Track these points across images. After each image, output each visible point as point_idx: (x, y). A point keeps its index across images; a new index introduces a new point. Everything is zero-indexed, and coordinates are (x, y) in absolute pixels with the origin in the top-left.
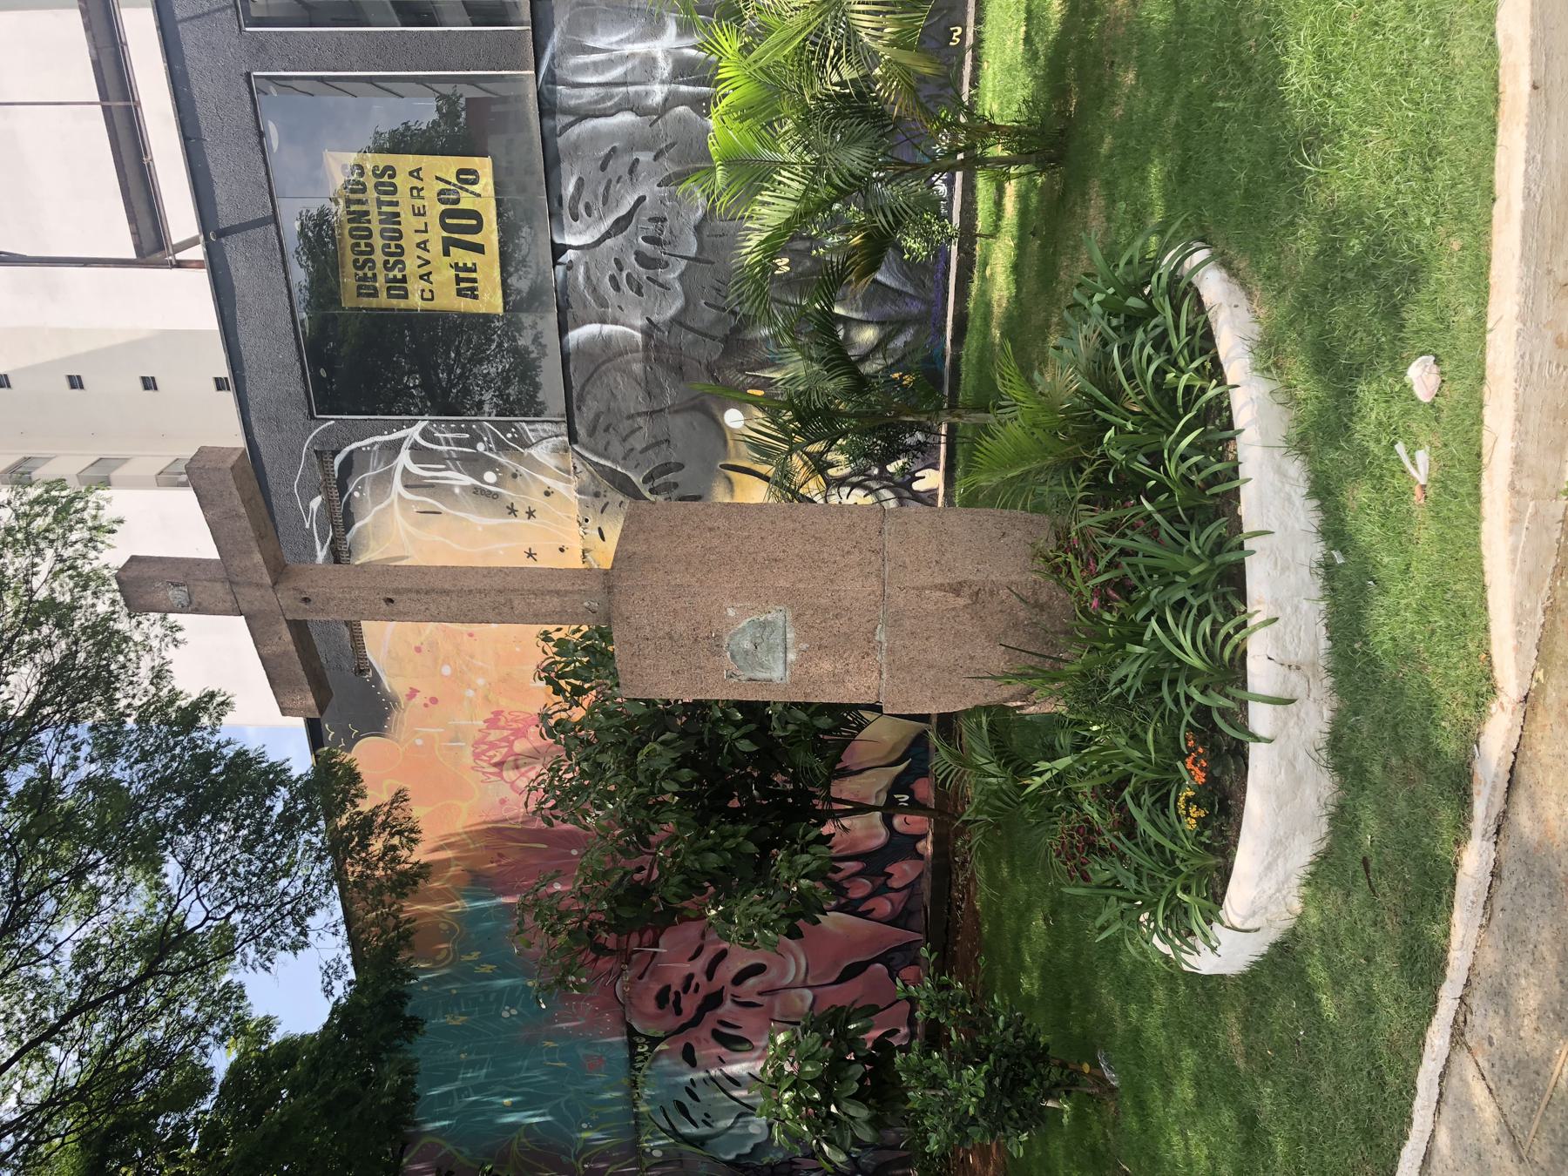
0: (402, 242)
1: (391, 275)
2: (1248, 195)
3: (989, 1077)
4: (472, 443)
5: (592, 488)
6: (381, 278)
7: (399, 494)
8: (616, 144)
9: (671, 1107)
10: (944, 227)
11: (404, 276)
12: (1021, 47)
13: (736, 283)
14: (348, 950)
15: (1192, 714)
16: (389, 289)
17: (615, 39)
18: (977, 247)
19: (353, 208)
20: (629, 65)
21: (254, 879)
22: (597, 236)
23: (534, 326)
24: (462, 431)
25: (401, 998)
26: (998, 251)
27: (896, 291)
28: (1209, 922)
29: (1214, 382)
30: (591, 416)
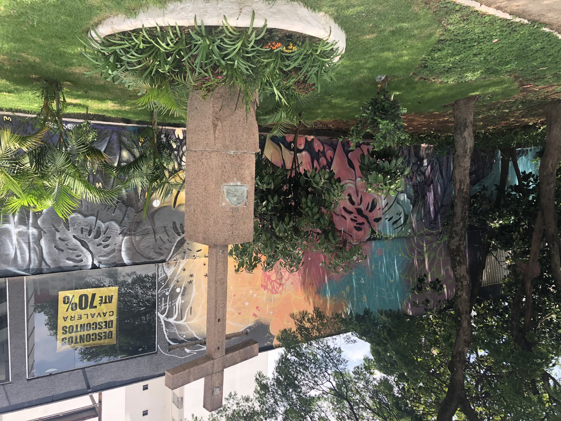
0: (92, 323)
1: (104, 327)
2: (70, 15)
3: (382, 119)
5: (182, 254)
6: (105, 330)
7: (185, 322)
8: (53, 246)
9: (395, 226)
10: (84, 126)
11: (104, 322)
12: (12, 94)
13: (106, 201)
14: (341, 335)
15: (258, 46)
16: (109, 327)
18: (92, 113)
19: (78, 340)
20: (21, 241)
21: (317, 366)
22: (89, 253)
23: (124, 277)
24: (161, 300)
25: (358, 316)
26: (93, 106)
27: (108, 143)
28: (328, 43)
29: (140, 32)
30: (156, 255)
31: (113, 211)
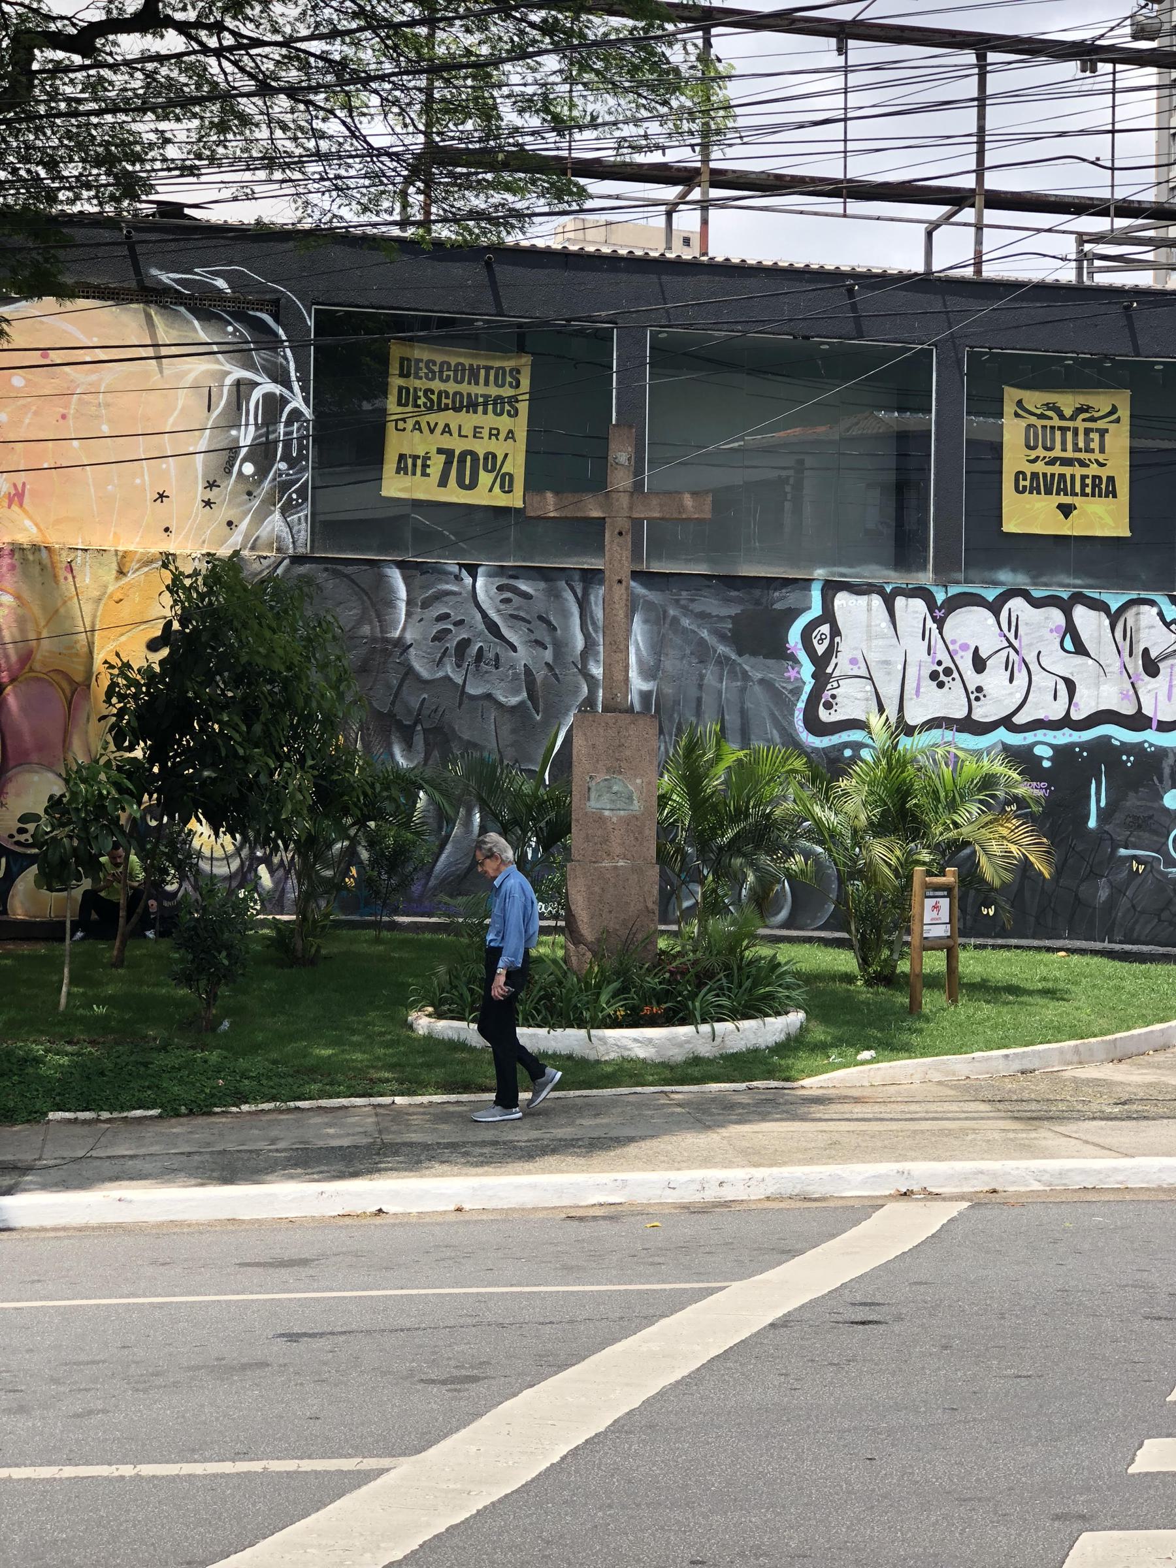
4: (286, 457)
7: (229, 373)
8: (559, 631)
17: (639, 638)
22: (484, 606)
31: (426, 705)
